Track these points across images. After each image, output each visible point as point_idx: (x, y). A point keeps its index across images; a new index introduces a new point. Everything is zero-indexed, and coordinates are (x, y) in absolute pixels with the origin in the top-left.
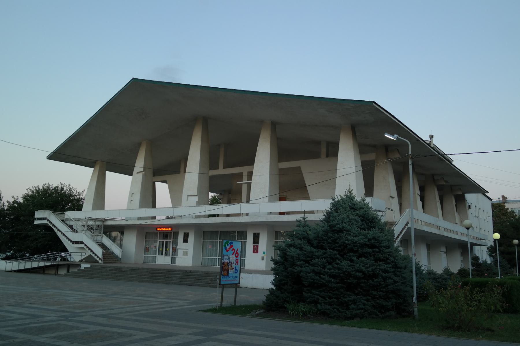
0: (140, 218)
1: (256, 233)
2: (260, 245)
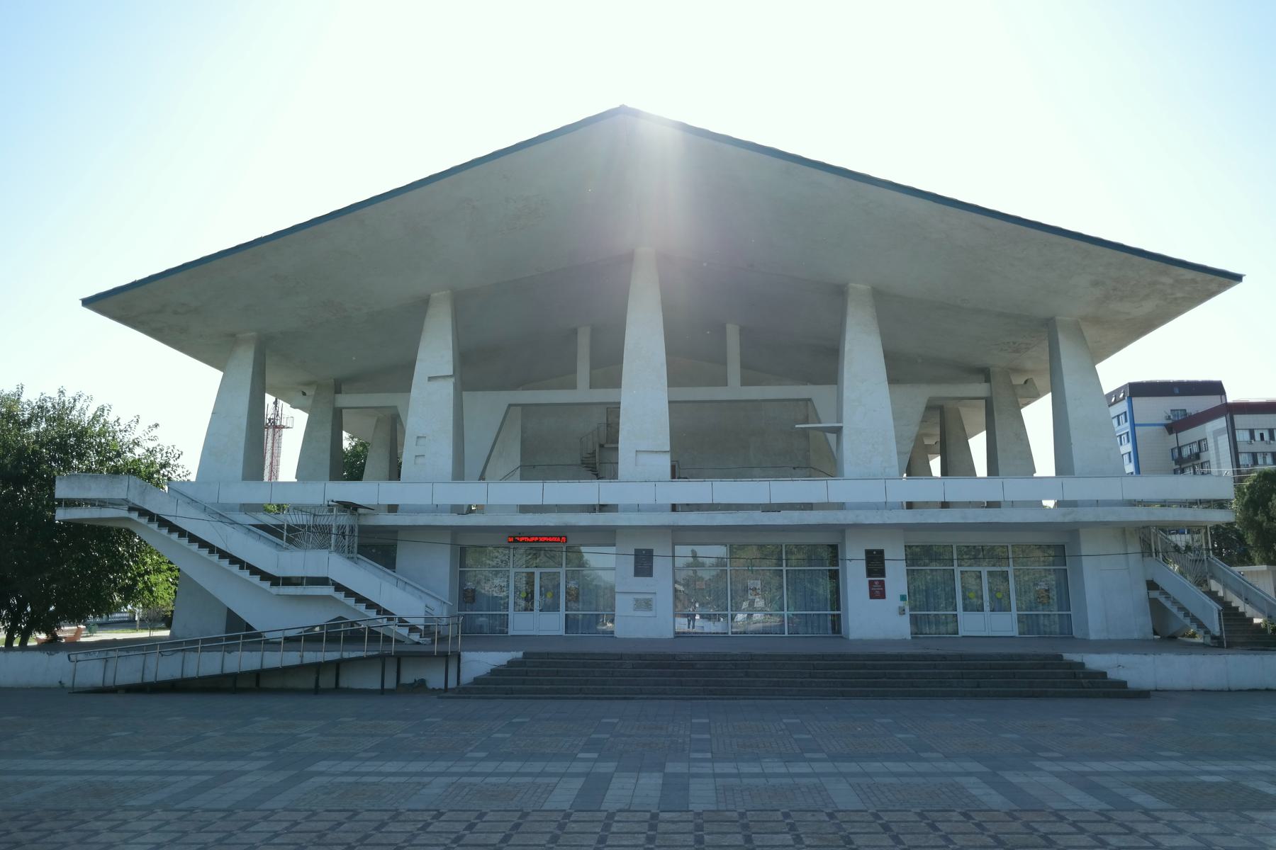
0: (524, 509)
1: (644, 550)
2: (888, 580)
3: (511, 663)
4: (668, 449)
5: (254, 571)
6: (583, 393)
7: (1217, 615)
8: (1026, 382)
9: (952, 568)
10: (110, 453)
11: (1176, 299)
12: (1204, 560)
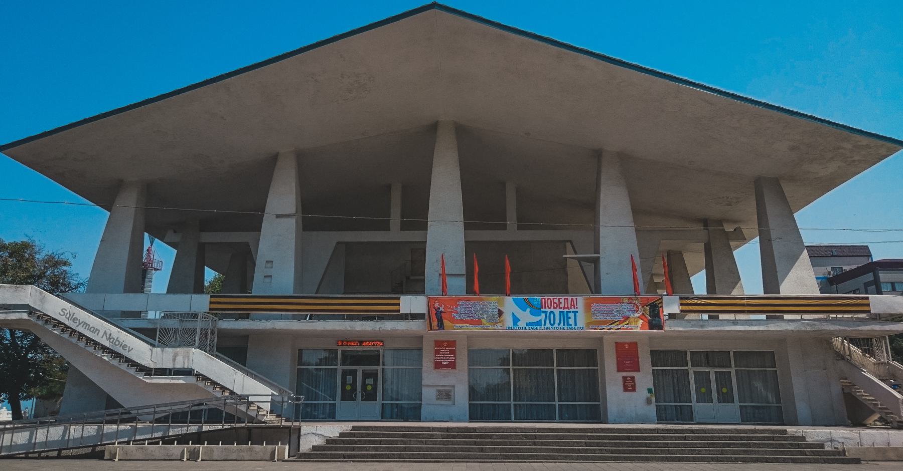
4: (464, 273)
6: (395, 234)
8: (735, 230)
9: (686, 368)
11: (854, 161)
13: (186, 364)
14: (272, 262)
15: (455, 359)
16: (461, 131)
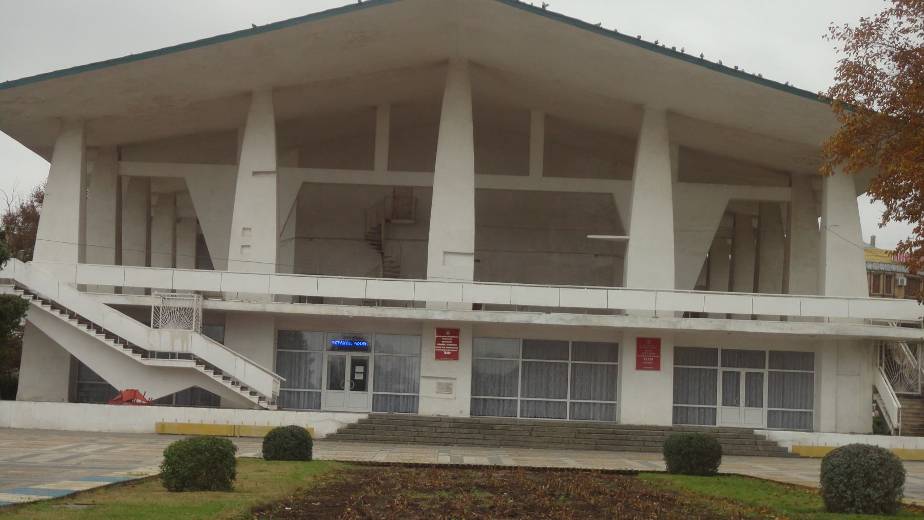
3: (361, 421)
4: (473, 251)
5: (126, 344)
7: (897, 412)
10: (353, 503)
12: (918, 371)
13: (185, 347)
14: (250, 229)
15: (458, 350)
16: (476, 67)
